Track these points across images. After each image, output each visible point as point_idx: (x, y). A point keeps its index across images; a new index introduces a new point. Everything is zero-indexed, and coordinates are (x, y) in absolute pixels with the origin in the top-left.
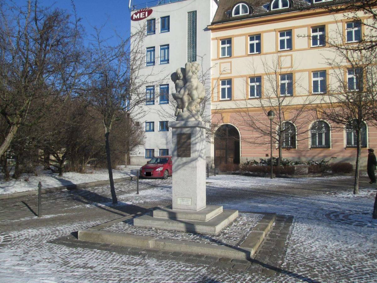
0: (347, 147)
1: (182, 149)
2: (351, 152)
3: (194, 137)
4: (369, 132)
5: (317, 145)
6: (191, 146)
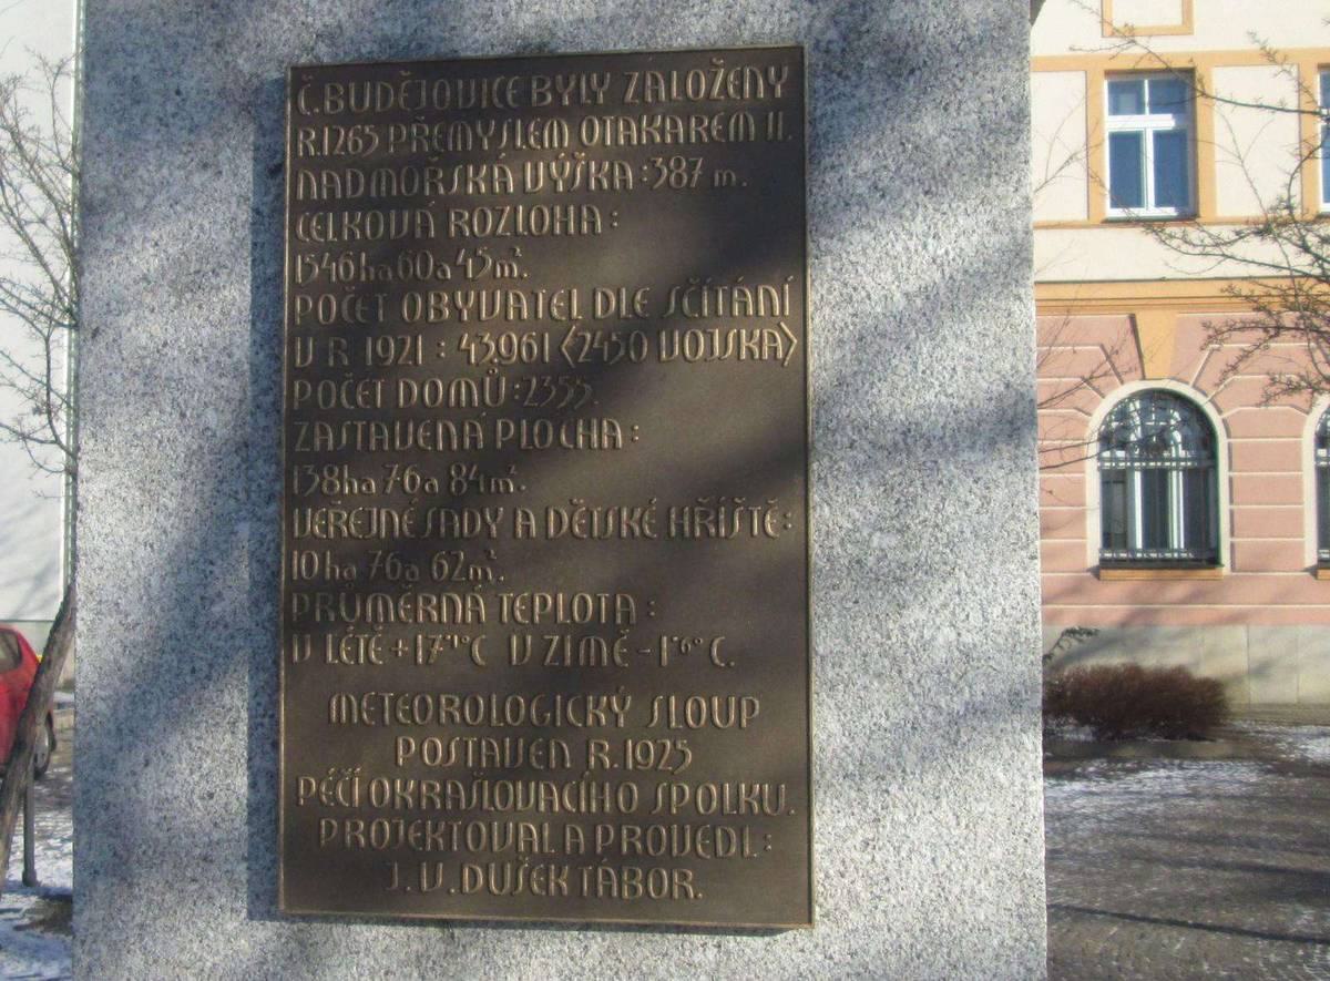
0: (1105, 564)
1: (460, 621)
2: (1133, 598)
3: (933, 181)
4: (1230, 468)
5: (1134, 551)
6: (838, 514)
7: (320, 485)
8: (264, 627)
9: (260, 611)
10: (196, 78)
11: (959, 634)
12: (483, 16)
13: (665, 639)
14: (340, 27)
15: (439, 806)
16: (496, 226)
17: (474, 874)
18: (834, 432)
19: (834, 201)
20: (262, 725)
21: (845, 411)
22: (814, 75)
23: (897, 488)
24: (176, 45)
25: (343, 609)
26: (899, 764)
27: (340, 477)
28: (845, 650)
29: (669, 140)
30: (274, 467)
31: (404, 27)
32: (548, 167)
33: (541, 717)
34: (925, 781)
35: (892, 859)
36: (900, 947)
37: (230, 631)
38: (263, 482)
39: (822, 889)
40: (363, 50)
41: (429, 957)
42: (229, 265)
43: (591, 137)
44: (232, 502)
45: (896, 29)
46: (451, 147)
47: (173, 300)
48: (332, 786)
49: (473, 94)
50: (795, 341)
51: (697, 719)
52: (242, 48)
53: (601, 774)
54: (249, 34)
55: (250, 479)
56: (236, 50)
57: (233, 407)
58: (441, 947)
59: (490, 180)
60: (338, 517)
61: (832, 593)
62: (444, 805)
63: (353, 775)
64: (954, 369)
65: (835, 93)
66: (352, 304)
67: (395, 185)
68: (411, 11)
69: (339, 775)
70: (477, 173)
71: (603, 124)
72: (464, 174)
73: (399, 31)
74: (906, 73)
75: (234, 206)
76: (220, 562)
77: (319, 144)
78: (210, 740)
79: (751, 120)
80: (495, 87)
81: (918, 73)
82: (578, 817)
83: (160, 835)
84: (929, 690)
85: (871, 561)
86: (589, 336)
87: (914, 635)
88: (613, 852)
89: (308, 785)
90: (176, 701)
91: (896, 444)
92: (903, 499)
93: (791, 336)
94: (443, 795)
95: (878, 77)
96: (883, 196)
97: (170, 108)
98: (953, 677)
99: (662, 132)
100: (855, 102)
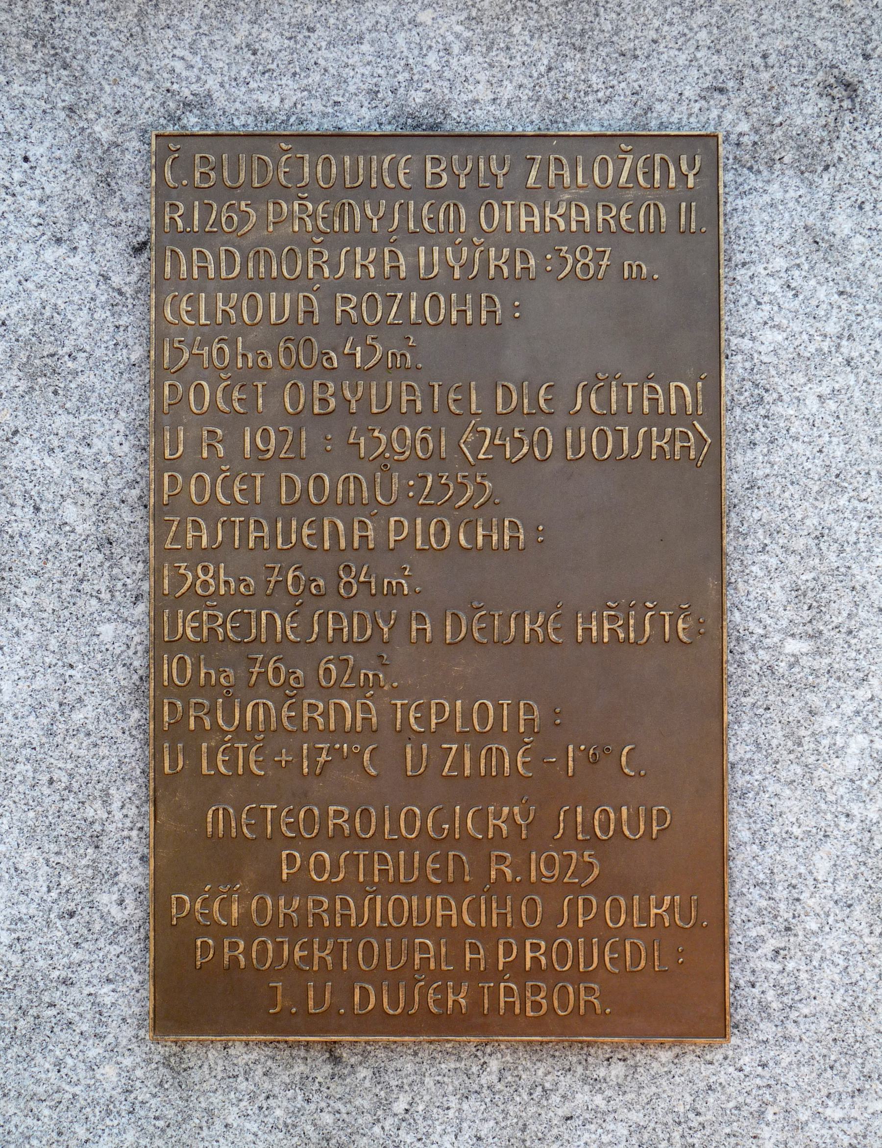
7: (193, 584)
8: (131, 735)
9: (127, 717)
10: (47, 144)
11: (872, 741)
12: (369, 92)
13: (571, 748)
14: (209, 95)
15: (327, 924)
16: (386, 314)
17: (364, 992)
18: (745, 536)
19: (745, 300)
20: (129, 838)
21: (756, 515)
22: (726, 170)
23: (810, 594)
24: (23, 106)
25: (219, 714)
26: (810, 872)
27: (216, 577)
28: (755, 757)
29: (574, 227)
30: (141, 565)
31: (282, 100)
32: (443, 252)
33: (439, 829)
34: (838, 889)
35: (803, 968)
36: (813, 1058)
37: (93, 739)
38: (129, 581)
39: (732, 1000)
40: (236, 123)
41: (314, 1079)
42: (88, 348)
43: (490, 222)
44: (94, 602)
45: (809, 122)
46: (337, 227)
47: (23, 386)
48: (206, 903)
49: (361, 171)
50: (709, 441)
51: (605, 828)
52: (99, 115)
53: (501, 886)
54: (107, 100)
55: (112, 578)
56: (92, 116)
57: (94, 501)
58: (327, 1069)
59: (379, 262)
60: (213, 618)
61: (743, 700)
62: (332, 921)
63: (230, 892)
64: (868, 474)
65: (747, 188)
66: (228, 391)
67: (275, 267)
68: (290, 82)
69: (214, 894)
70: (365, 256)
71: (503, 206)
72: (351, 254)
73: (276, 103)
74: (820, 169)
75: (93, 287)
76: (81, 666)
77: (188, 217)
78: (70, 855)
79: (663, 211)
80: (386, 165)
81: (832, 169)
82: (476, 932)
83: (13, 958)
84: (842, 797)
85: (783, 667)
86: (488, 431)
87: (826, 742)
88: (516, 968)
89: (181, 903)
90: (31, 814)
91: (808, 549)
92: (815, 604)
93: (705, 435)
94: (331, 911)
95: (791, 172)
96: (796, 295)
97: (17, 176)
98: (865, 785)
99: (566, 217)
100: (767, 198)
